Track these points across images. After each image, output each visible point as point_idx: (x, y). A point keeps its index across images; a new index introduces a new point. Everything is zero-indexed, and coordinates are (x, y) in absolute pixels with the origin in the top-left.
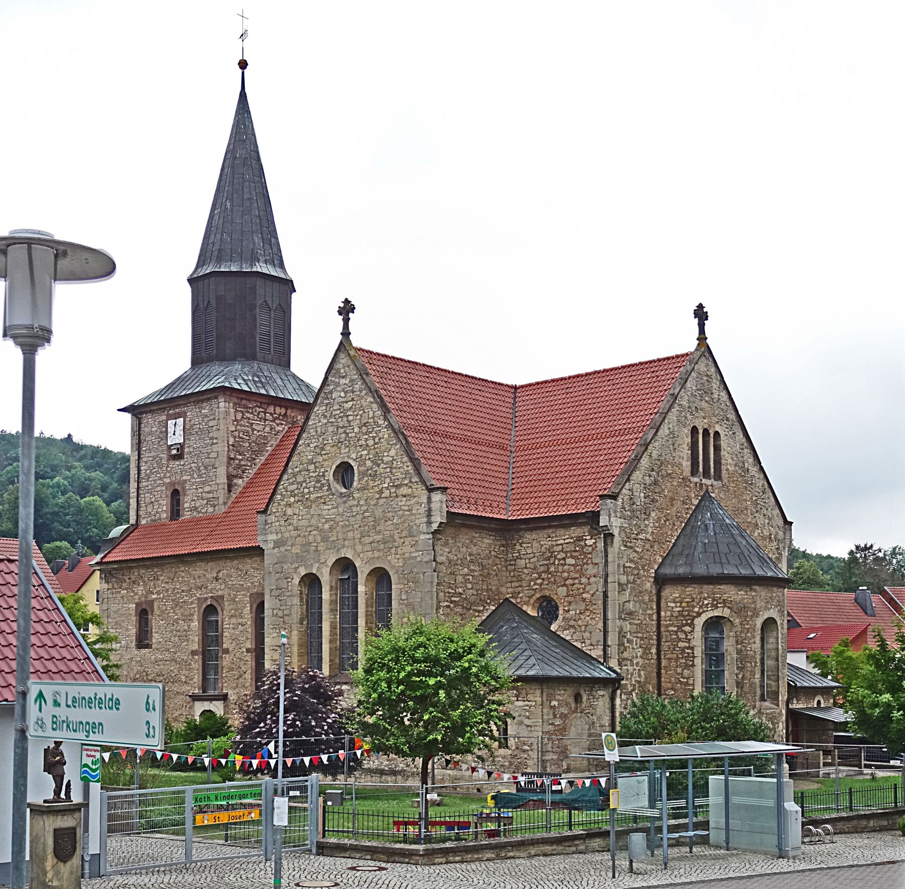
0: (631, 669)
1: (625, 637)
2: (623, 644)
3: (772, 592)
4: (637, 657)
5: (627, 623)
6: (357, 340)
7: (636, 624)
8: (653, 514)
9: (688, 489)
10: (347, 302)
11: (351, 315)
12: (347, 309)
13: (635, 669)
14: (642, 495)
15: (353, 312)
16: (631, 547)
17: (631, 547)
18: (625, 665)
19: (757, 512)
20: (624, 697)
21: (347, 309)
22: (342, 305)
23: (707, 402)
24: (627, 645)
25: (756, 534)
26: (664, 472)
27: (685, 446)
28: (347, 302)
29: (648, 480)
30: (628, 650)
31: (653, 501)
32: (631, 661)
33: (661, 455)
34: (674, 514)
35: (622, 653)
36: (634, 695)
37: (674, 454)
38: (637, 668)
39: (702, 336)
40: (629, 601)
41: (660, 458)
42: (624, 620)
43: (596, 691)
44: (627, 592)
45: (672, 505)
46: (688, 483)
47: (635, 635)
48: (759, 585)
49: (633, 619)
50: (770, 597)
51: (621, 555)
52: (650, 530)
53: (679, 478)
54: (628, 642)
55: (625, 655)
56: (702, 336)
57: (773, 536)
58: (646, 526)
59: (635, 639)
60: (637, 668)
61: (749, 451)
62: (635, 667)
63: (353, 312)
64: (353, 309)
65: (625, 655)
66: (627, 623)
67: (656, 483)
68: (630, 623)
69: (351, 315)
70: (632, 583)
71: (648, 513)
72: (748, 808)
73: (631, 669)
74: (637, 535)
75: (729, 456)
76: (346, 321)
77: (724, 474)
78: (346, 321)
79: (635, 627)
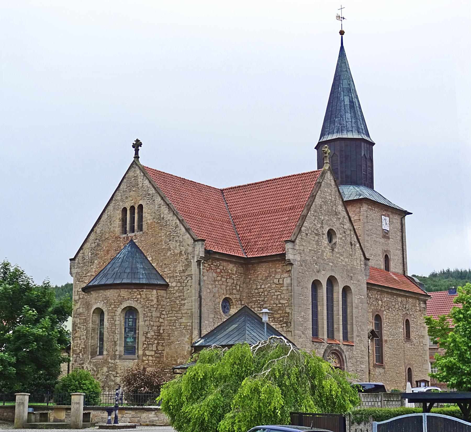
0: (79, 342)
1: (77, 326)
2: (76, 330)
3: (99, 293)
4: (83, 336)
5: (78, 319)
6: (143, 161)
7: (83, 319)
8: (96, 262)
9: (119, 242)
10: (137, 141)
11: (139, 148)
12: (137, 145)
13: (82, 342)
14: (90, 253)
15: (141, 146)
16: (82, 281)
17: (82, 281)
18: (76, 340)
19: (170, 241)
20: (74, 356)
21: (137, 145)
22: (135, 143)
23: (134, 191)
24: (77, 330)
25: (168, 254)
26: (104, 238)
27: (118, 221)
28: (137, 141)
29: (93, 245)
30: (78, 332)
31: (96, 255)
32: (80, 337)
33: (102, 230)
34: (109, 258)
35: (75, 334)
36: (81, 354)
37: (110, 227)
38: (83, 341)
39: (137, 156)
40: (79, 308)
41: (102, 232)
42: (76, 317)
43: (63, 353)
44: (79, 304)
45: (108, 254)
46: (119, 239)
47: (82, 324)
48: (93, 290)
49: (82, 316)
50: (98, 296)
51: (76, 286)
52: (94, 270)
53: (113, 238)
54: (78, 328)
55: (77, 335)
56: (137, 156)
57: (183, 252)
58: (91, 268)
59: (82, 326)
60: (83, 341)
61: (165, 207)
62: (82, 341)
63: (141, 146)
64: (140, 145)
65: (77, 335)
66: (78, 319)
67: (98, 245)
68: (80, 319)
69: (139, 148)
70: (82, 299)
71: (93, 262)
72: (80, 398)
73: (79, 342)
74: (86, 274)
75: (149, 215)
76: (137, 151)
77: (145, 227)
78: (137, 151)
79: (83, 320)
